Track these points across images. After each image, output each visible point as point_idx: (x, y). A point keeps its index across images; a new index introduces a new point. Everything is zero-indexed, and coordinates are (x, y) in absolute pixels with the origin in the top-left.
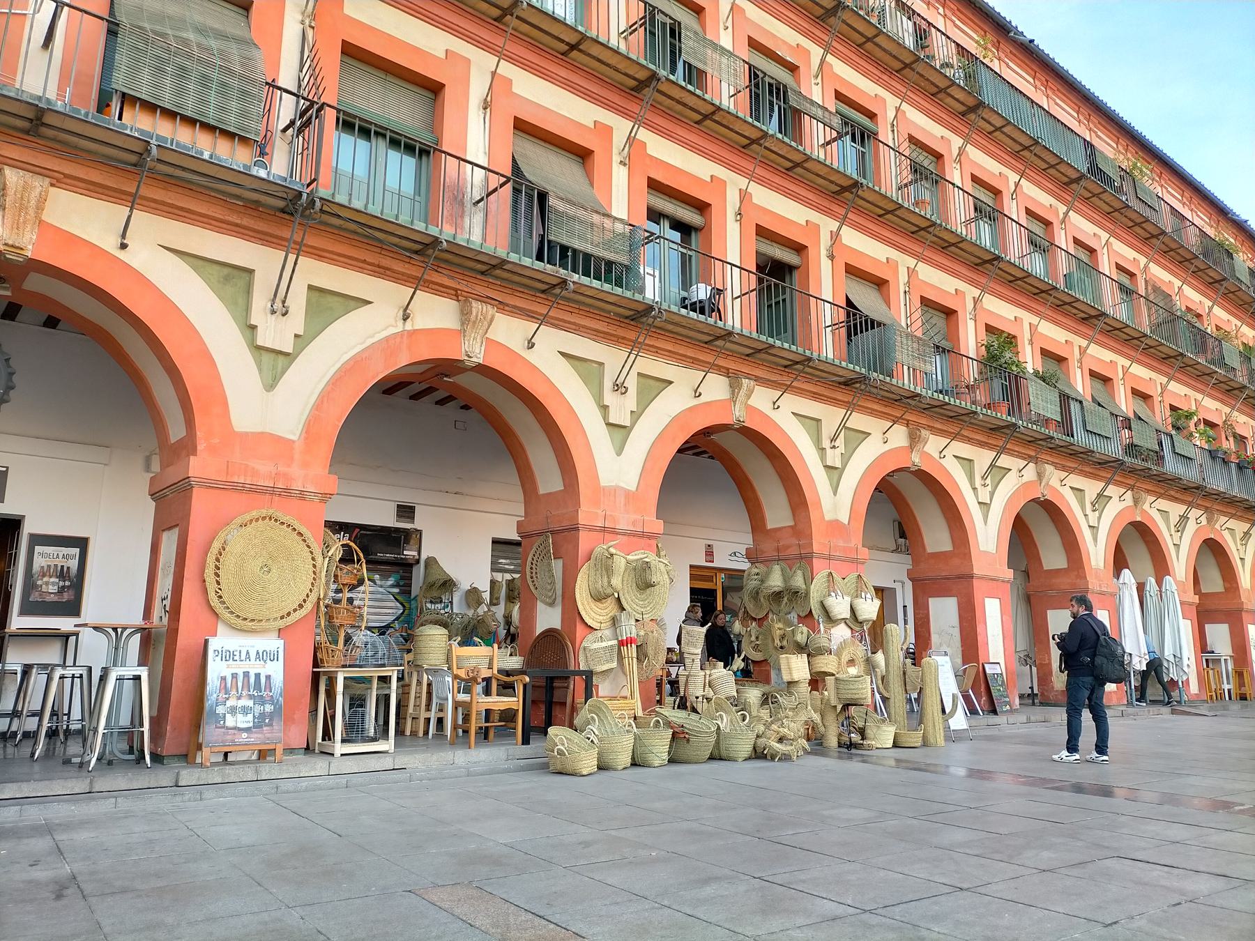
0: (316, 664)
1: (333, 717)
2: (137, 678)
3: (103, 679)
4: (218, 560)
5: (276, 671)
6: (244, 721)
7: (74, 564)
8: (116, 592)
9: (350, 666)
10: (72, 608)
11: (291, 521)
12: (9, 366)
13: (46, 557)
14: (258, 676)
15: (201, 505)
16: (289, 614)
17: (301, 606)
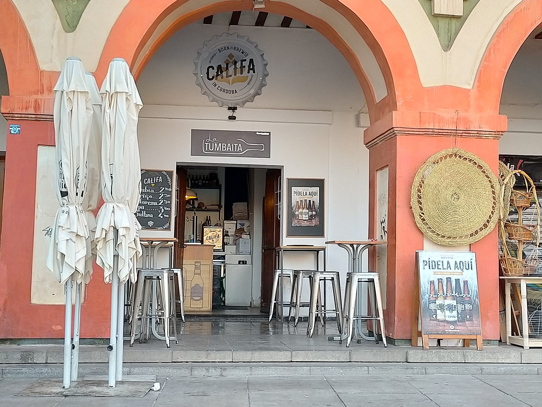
0: (501, 274)
1: (519, 316)
2: (372, 281)
3: (349, 281)
4: (419, 191)
5: (470, 276)
6: (451, 316)
7: (316, 199)
8: (347, 219)
9: (531, 275)
10: (318, 231)
11: (472, 157)
12: (264, 60)
13: (300, 194)
14: (457, 281)
15: (403, 147)
16: (476, 232)
17: (485, 226)
